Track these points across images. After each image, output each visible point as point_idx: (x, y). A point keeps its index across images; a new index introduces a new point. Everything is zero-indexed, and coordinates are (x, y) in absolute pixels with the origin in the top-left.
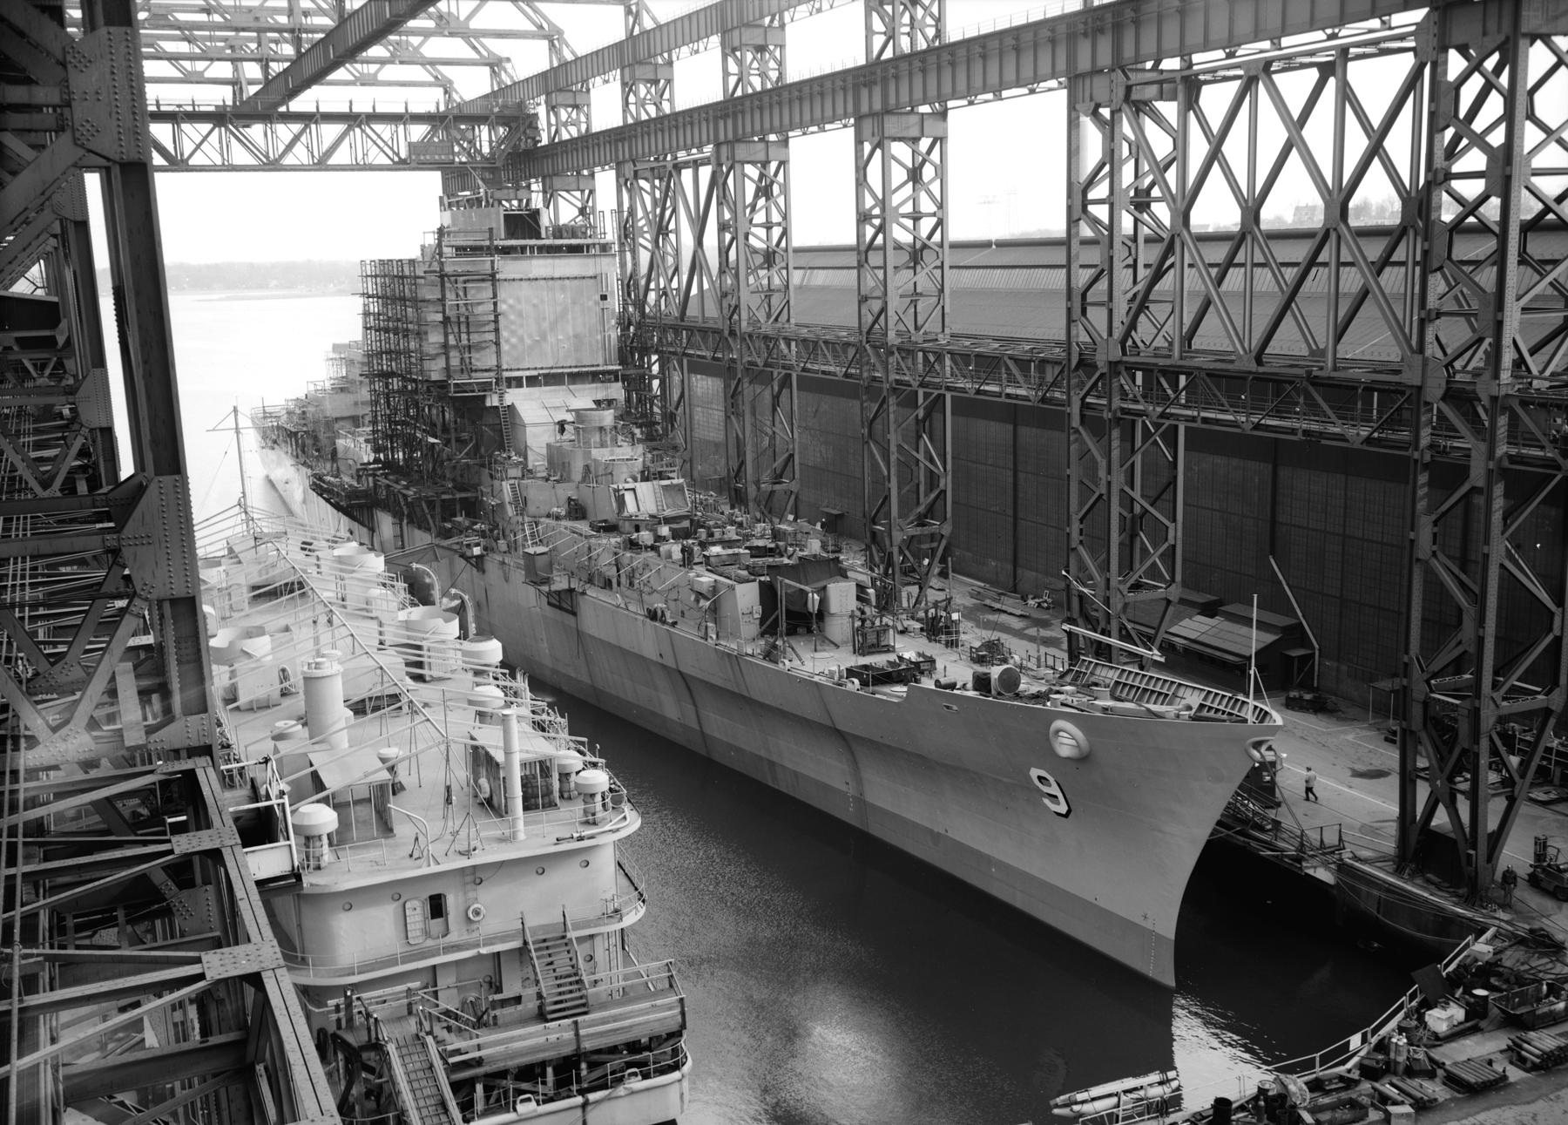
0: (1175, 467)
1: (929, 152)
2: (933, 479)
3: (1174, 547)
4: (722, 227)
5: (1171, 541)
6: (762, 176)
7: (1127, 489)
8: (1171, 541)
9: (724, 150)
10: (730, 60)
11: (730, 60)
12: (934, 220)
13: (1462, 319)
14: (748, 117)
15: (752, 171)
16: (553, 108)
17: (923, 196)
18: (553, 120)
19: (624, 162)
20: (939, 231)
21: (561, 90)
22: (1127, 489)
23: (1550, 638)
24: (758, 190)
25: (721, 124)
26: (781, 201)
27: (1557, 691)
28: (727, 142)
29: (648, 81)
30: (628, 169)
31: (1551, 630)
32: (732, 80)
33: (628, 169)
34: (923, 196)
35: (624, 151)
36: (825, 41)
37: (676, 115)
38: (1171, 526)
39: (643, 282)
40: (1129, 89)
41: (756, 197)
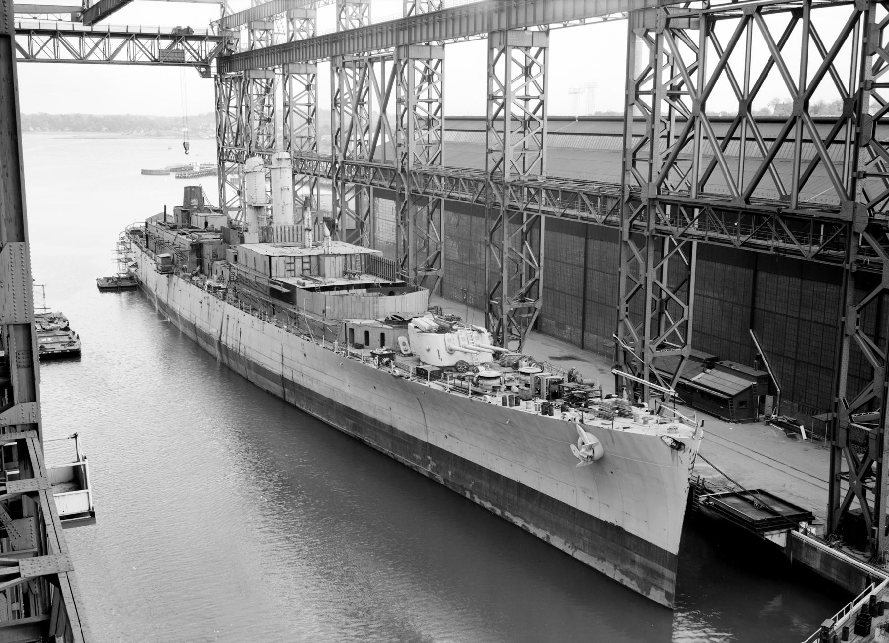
0: (690, 269)
8: (685, 317)
9: (402, 50)
15: (420, 65)
16: (292, 20)
18: (291, 27)
19: (336, 56)
23: (682, 320)
30: (339, 61)
33: (339, 61)
36: (326, 22)
37: (371, 27)
38: (686, 307)
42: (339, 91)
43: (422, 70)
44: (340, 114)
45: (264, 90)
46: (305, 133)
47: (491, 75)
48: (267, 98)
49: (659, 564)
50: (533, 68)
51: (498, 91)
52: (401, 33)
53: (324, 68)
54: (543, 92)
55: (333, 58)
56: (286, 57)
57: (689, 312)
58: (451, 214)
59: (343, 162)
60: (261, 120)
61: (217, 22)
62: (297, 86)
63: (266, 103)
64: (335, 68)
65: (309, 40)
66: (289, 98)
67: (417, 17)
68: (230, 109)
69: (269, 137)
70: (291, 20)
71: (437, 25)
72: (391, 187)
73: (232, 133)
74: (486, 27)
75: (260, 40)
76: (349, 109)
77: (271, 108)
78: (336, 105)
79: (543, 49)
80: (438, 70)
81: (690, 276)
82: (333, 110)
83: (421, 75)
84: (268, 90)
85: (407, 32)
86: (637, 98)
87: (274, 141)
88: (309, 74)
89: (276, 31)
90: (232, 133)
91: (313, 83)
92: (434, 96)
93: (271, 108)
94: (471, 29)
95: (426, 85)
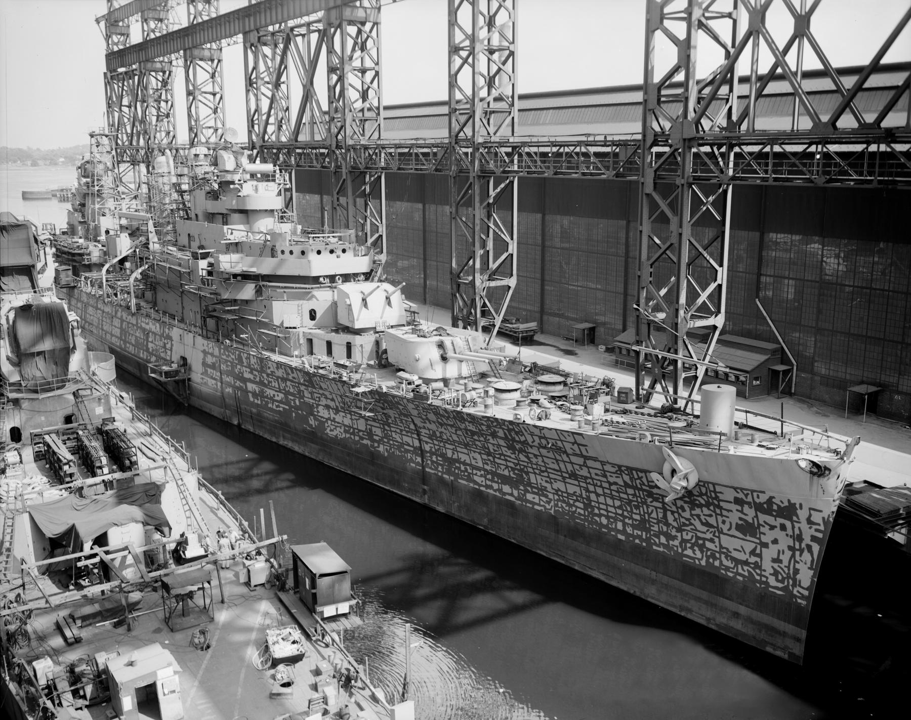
0: (724, 225)
1: (371, 31)
2: (375, 228)
3: (720, 286)
4: (331, 70)
5: (510, 251)
6: (360, 32)
7: (486, 220)
8: (719, 281)
9: (188, 52)
10: (191, 6)
11: (191, 6)
12: (373, 73)
13: (714, 102)
14: (263, 15)
15: (352, 30)
16: (146, 20)
17: (367, 58)
18: (146, 28)
19: (250, 31)
20: (511, 58)
21: (149, 9)
22: (486, 220)
23: (716, 284)
24: (356, 43)
25: (247, 20)
26: (374, 53)
27: (720, 316)
28: (189, 48)
29: (156, 19)
30: (253, 37)
31: (716, 280)
32: (192, 17)
33: (253, 37)
34: (367, 58)
35: (250, 23)
36: (179, 17)
37: (219, 18)
38: (719, 269)
39: (264, 117)
40: (259, 38)
41: (353, 50)
42: (254, 68)
43: (354, 35)
44: (256, 96)
45: (160, 84)
46: (212, 123)
47: (453, 22)
48: (164, 92)
49: (779, 618)
50: (368, 43)
51: (463, 41)
52: (247, 20)
53: (177, 61)
54: (377, 64)
55: (245, 34)
56: (188, 42)
57: (722, 275)
58: (301, 195)
59: (261, 147)
60: (158, 116)
61: (103, 16)
62: (202, 75)
63: (163, 97)
64: (248, 45)
65: (163, 36)
66: (193, 85)
67: (199, 24)
68: (123, 108)
69: (168, 133)
70: (145, 20)
71: (237, 22)
72: (323, 167)
73: (127, 133)
74: (323, 5)
75: (117, 44)
76: (266, 91)
77: (170, 103)
78: (251, 85)
79: (376, 24)
80: (374, 33)
81: (724, 232)
82: (248, 91)
83: (352, 41)
84: (165, 83)
85: (252, 19)
86: (662, 22)
87: (174, 137)
88: (212, 61)
89: (171, 21)
90: (127, 133)
91: (219, 69)
92: (368, 64)
93: (170, 103)
94: (232, 32)
95: (358, 53)
